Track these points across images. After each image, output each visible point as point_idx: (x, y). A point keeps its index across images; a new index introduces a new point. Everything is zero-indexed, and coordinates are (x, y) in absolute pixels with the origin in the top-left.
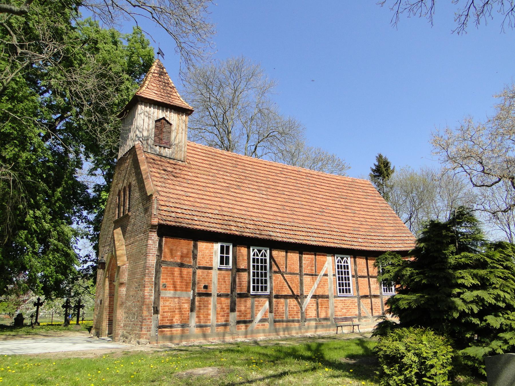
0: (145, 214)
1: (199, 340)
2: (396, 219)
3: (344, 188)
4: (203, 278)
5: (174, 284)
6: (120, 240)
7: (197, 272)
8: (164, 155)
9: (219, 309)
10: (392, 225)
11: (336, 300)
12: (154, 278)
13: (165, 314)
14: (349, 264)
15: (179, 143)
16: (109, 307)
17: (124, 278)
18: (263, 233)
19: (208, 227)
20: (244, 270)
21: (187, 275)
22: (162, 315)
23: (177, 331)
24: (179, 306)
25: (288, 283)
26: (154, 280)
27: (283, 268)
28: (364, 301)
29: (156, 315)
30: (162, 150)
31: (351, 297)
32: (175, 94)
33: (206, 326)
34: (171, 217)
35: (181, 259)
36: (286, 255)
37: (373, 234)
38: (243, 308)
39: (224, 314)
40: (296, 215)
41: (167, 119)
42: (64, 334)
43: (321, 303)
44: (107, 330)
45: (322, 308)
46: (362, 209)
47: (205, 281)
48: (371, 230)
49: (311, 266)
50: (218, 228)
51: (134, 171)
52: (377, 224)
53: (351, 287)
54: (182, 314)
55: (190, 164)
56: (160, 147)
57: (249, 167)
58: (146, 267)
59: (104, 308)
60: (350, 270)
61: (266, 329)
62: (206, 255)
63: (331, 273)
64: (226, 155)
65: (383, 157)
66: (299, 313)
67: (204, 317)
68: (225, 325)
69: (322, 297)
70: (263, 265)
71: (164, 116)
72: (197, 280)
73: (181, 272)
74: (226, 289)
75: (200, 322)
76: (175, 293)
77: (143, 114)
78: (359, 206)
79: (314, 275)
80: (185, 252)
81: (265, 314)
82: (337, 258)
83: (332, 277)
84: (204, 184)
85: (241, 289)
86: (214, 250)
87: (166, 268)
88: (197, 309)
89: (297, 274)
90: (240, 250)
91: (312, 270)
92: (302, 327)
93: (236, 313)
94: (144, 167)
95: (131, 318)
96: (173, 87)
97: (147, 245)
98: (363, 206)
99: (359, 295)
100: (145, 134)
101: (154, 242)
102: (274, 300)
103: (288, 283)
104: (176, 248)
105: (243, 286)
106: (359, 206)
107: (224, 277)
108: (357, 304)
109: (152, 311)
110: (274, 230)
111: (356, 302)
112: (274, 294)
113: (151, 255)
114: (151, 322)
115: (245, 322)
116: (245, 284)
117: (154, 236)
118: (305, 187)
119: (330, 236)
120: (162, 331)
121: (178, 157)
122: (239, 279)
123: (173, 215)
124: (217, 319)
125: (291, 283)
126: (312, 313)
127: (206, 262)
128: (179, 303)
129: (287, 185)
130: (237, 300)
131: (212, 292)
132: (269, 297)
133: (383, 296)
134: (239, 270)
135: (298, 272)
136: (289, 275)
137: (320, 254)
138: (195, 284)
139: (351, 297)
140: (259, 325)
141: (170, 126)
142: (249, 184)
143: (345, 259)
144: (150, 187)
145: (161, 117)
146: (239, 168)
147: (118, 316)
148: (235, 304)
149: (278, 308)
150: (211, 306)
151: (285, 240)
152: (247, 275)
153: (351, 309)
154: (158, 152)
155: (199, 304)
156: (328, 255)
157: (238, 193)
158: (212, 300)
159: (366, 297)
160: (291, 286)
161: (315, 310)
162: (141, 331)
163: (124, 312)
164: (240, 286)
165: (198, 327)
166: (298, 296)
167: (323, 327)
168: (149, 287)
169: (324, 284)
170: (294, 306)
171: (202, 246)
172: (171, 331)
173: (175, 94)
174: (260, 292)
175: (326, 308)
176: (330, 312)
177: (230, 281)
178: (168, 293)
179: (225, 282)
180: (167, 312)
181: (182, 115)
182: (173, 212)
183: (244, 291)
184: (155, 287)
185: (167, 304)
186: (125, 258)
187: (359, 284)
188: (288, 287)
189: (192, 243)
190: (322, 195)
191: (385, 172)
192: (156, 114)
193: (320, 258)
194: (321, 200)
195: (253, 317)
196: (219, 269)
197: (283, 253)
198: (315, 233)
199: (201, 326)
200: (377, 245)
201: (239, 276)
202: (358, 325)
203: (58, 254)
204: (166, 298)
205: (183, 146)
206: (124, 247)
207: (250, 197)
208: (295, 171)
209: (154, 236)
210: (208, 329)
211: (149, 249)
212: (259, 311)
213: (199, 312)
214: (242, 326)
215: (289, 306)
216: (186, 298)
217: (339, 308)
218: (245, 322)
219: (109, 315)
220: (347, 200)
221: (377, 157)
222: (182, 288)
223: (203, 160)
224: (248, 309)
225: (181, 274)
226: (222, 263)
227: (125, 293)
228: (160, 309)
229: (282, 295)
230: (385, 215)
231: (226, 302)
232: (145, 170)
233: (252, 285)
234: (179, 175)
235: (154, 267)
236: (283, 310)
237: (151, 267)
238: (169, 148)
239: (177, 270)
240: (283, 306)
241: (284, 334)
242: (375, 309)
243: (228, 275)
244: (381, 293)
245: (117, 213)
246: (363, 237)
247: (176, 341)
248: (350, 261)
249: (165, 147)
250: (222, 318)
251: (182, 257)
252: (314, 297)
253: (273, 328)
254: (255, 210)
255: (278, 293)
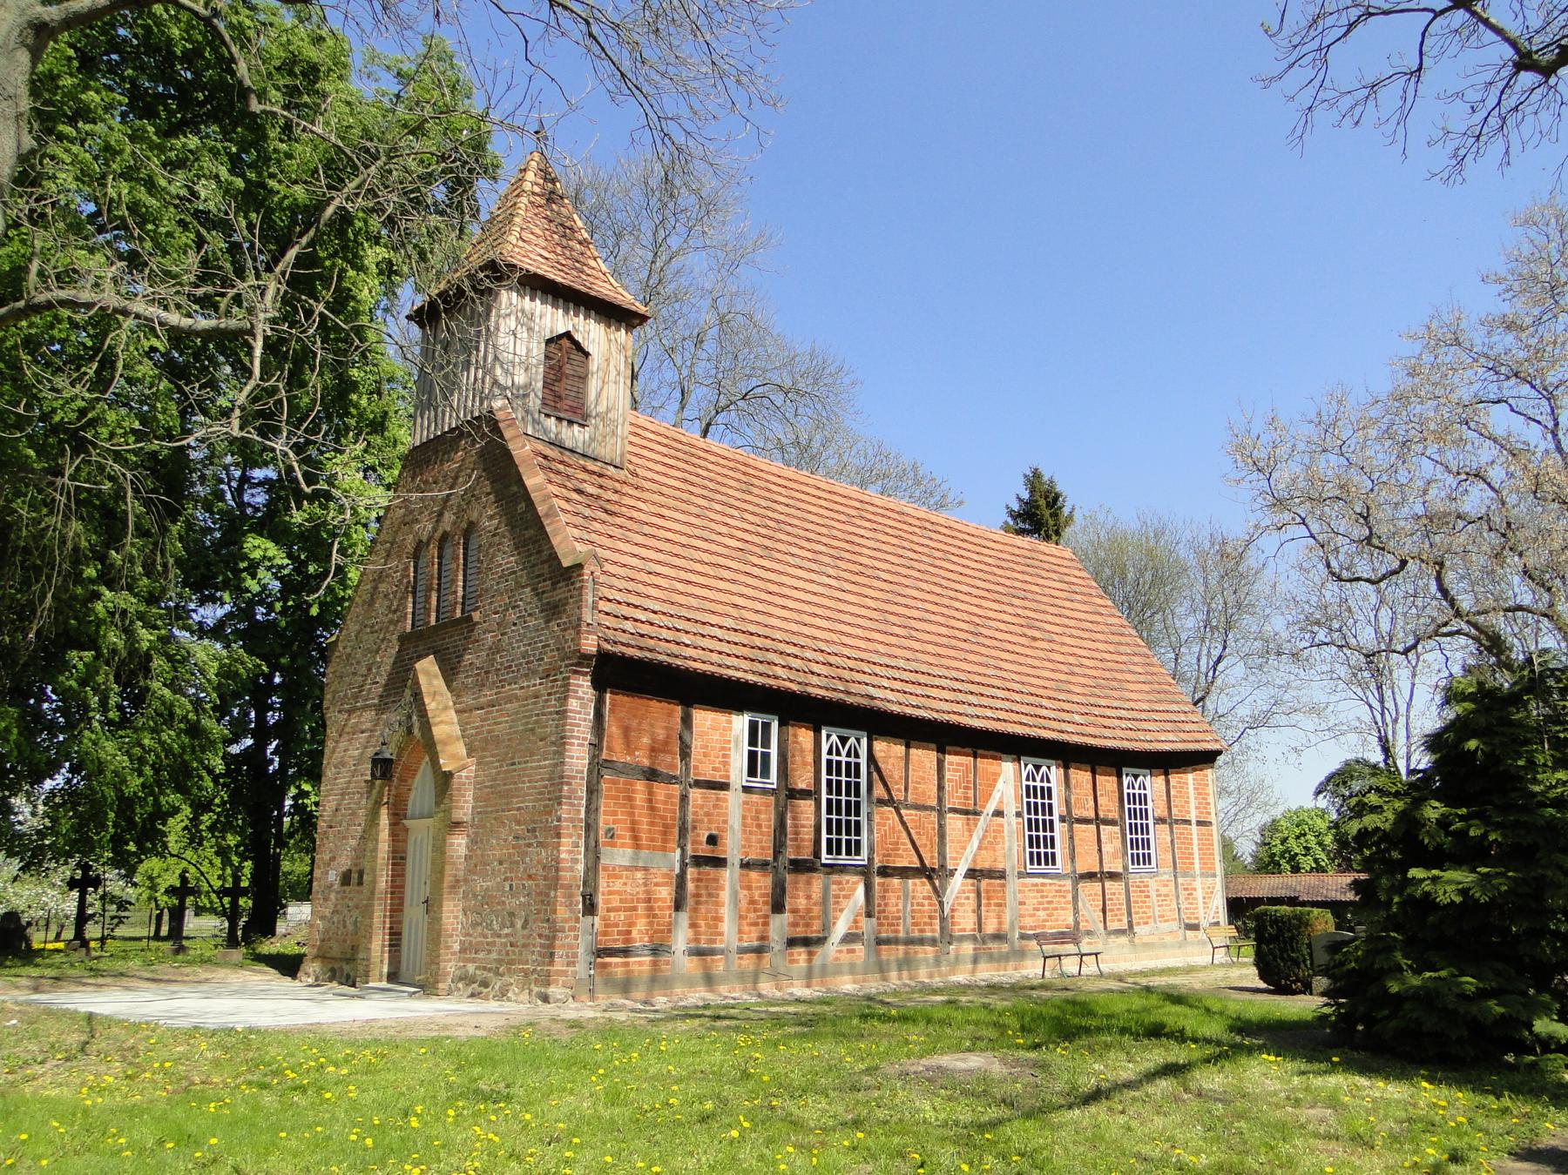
0: (547, 622)
1: (695, 992)
2: (1148, 661)
3: (1015, 566)
4: (708, 814)
5: (633, 830)
6: (435, 693)
7: (691, 796)
8: (568, 444)
9: (744, 904)
10: (1142, 678)
11: (1024, 885)
12: (583, 810)
13: (612, 914)
14: (1053, 785)
15: (608, 410)
16: (392, 893)
17: (463, 808)
18: (854, 688)
19: (720, 666)
20: (805, 794)
21: (666, 803)
22: (604, 919)
23: (641, 963)
24: (648, 892)
25: (909, 834)
26: (583, 816)
27: (899, 790)
28: (1091, 889)
29: (590, 918)
30: (564, 430)
31: (1057, 876)
32: (592, 263)
33: (712, 952)
34: (624, 631)
35: (650, 757)
36: (907, 754)
37: (1103, 702)
38: (802, 903)
39: (758, 917)
40: (918, 640)
41: (578, 337)
42: (208, 975)
43: (987, 891)
44: (386, 961)
45: (989, 905)
46: (1067, 631)
47: (710, 822)
48: (1097, 691)
49: (967, 788)
50: (745, 671)
51: (489, 490)
52: (1107, 674)
53: (1057, 850)
54: (655, 916)
55: (637, 476)
56: (559, 419)
57: (780, 494)
58: (562, 777)
59: (377, 896)
60: (1055, 801)
61: (858, 962)
62: (713, 748)
63: (1011, 808)
64: (720, 456)
65: (1046, 478)
66: (934, 918)
67: (708, 926)
68: (759, 951)
69: (991, 874)
70: (852, 779)
71: (571, 329)
72: (690, 818)
73: (651, 793)
74: (762, 848)
75: (697, 940)
76: (636, 854)
77: (513, 318)
78: (1057, 620)
79: (971, 813)
80: (661, 737)
81: (855, 921)
82: (1026, 765)
83: (1014, 820)
84: (683, 540)
85: (798, 847)
86: (733, 733)
87: (614, 783)
88: (690, 901)
89: (932, 808)
90: (795, 736)
91: (967, 798)
92: (943, 958)
93: (786, 917)
94: (534, 480)
95: (496, 927)
96: (585, 240)
97: (565, 711)
98: (1066, 621)
99: (1074, 871)
100: (520, 378)
101: (583, 706)
102: (877, 880)
103: (909, 834)
104: (640, 724)
105: (802, 840)
106: (1057, 620)
107: (758, 812)
108: (1070, 897)
109: (580, 906)
110: (876, 680)
111: (1067, 891)
112: (877, 864)
113: (576, 742)
114: (576, 937)
115: (806, 942)
116: (807, 834)
117: (583, 687)
118: (924, 558)
119: (1007, 705)
120: (605, 966)
121: (605, 452)
122: (794, 818)
123: (628, 626)
124: (740, 932)
125: (918, 833)
126: (965, 922)
127: (714, 769)
128: (645, 885)
129: (880, 550)
130: (789, 878)
131: (728, 856)
132: (865, 872)
133: (1130, 876)
134: (794, 794)
135: (934, 803)
136: (913, 812)
137: (986, 753)
138: (686, 829)
139: (1057, 876)
140: (840, 951)
141: (584, 359)
142: (790, 544)
143: (1044, 769)
144: (568, 541)
145: (562, 331)
146: (757, 496)
147: (444, 920)
148: (783, 890)
149: (886, 905)
150: (725, 896)
151: (909, 711)
152: (813, 808)
153: (1056, 909)
154: (553, 436)
155: (697, 887)
156: (1004, 756)
157: (769, 570)
158: (728, 876)
159: (1090, 876)
160: (918, 843)
161: (974, 911)
162: (551, 963)
163: (460, 908)
164: (796, 840)
165: (694, 954)
166: (933, 870)
167: (991, 958)
168: (570, 836)
169: (995, 837)
170: (924, 898)
171: (704, 718)
172: (627, 964)
173: (592, 263)
174: (843, 859)
175: (1000, 905)
176: (1007, 916)
177: (772, 823)
178: (618, 856)
179: (759, 826)
180: (617, 910)
181: (618, 330)
182: (626, 618)
183: (806, 854)
184: (587, 837)
185: (618, 885)
186: (462, 750)
187: (1076, 839)
188: (910, 846)
189: (678, 710)
190: (968, 585)
191: (1051, 522)
192: (547, 320)
193: (985, 765)
194: (967, 598)
195: (827, 927)
196: (746, 789)
197: (899, 749)
198: (972, 693)
199: (699, 953)
200: (1119, 733)
201: (792, 812)
202: (1096, 954)
203: (172, 733)
204: (614, 869)
205: (620, 421)
206: (452, 714)
207: (801, 584)
208: (893, 510)
209: (582, 686)
210: (717, 961)
211: (571, 725)
212: (841, 910)
213: (695, 910)
214: (800, 954)
215: (913, 898)
216: (665, 870)
217: (1029, 907)
218: (806, 942)
219: (391, 917)
220: (1027, 604)
221: (1025, 476)
222: (652, 840)
223: (665, 464)
224: (815, 904)
225: (650, 801)
226: (752, 772)
227: (463, 851)
228: (600, 900)
229: (895, 868)
230: (1122, 649)
231: (762, 882)
232: (540, 488)
233: (824, 836)
234: (615, 508)
235: (582, 778)
236: (898, 911)
237: (575, 777)
238: (583, 426)
239: (640, 786)
240: (899, 898)
241: (900, 978)
242: (1112, 910)
243: (767, 805)
244: (1126, 868)
245: (410, 610)
246: (1084, 710)
247: (639, 994)
248: (1055, 773)
249: (571, 422)
250: (753, 928)
251: (654, 750)
252: (972, 873)
253: (873, 959)
254: (818, 622)
255: (888, 861)
